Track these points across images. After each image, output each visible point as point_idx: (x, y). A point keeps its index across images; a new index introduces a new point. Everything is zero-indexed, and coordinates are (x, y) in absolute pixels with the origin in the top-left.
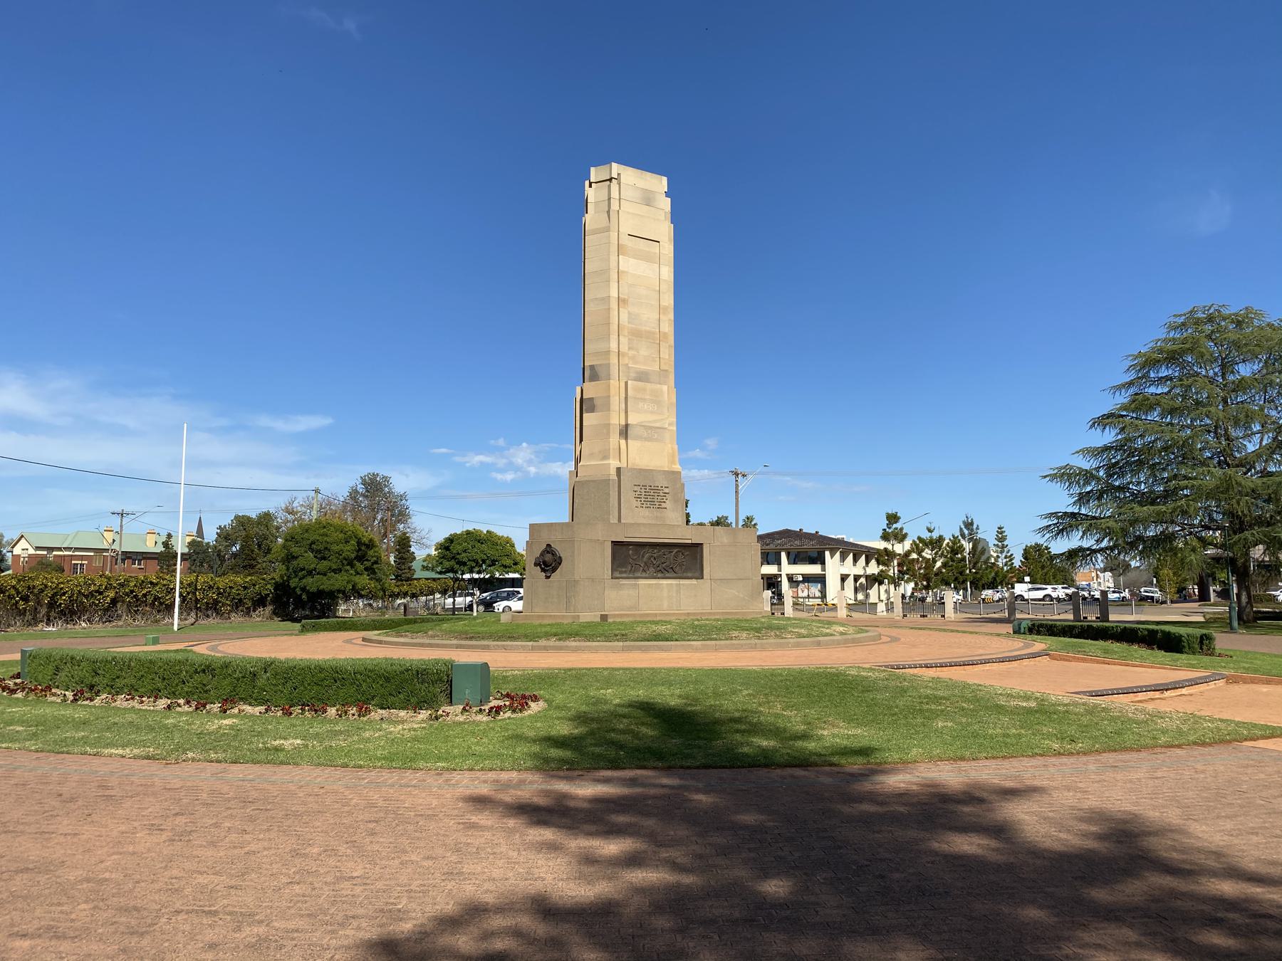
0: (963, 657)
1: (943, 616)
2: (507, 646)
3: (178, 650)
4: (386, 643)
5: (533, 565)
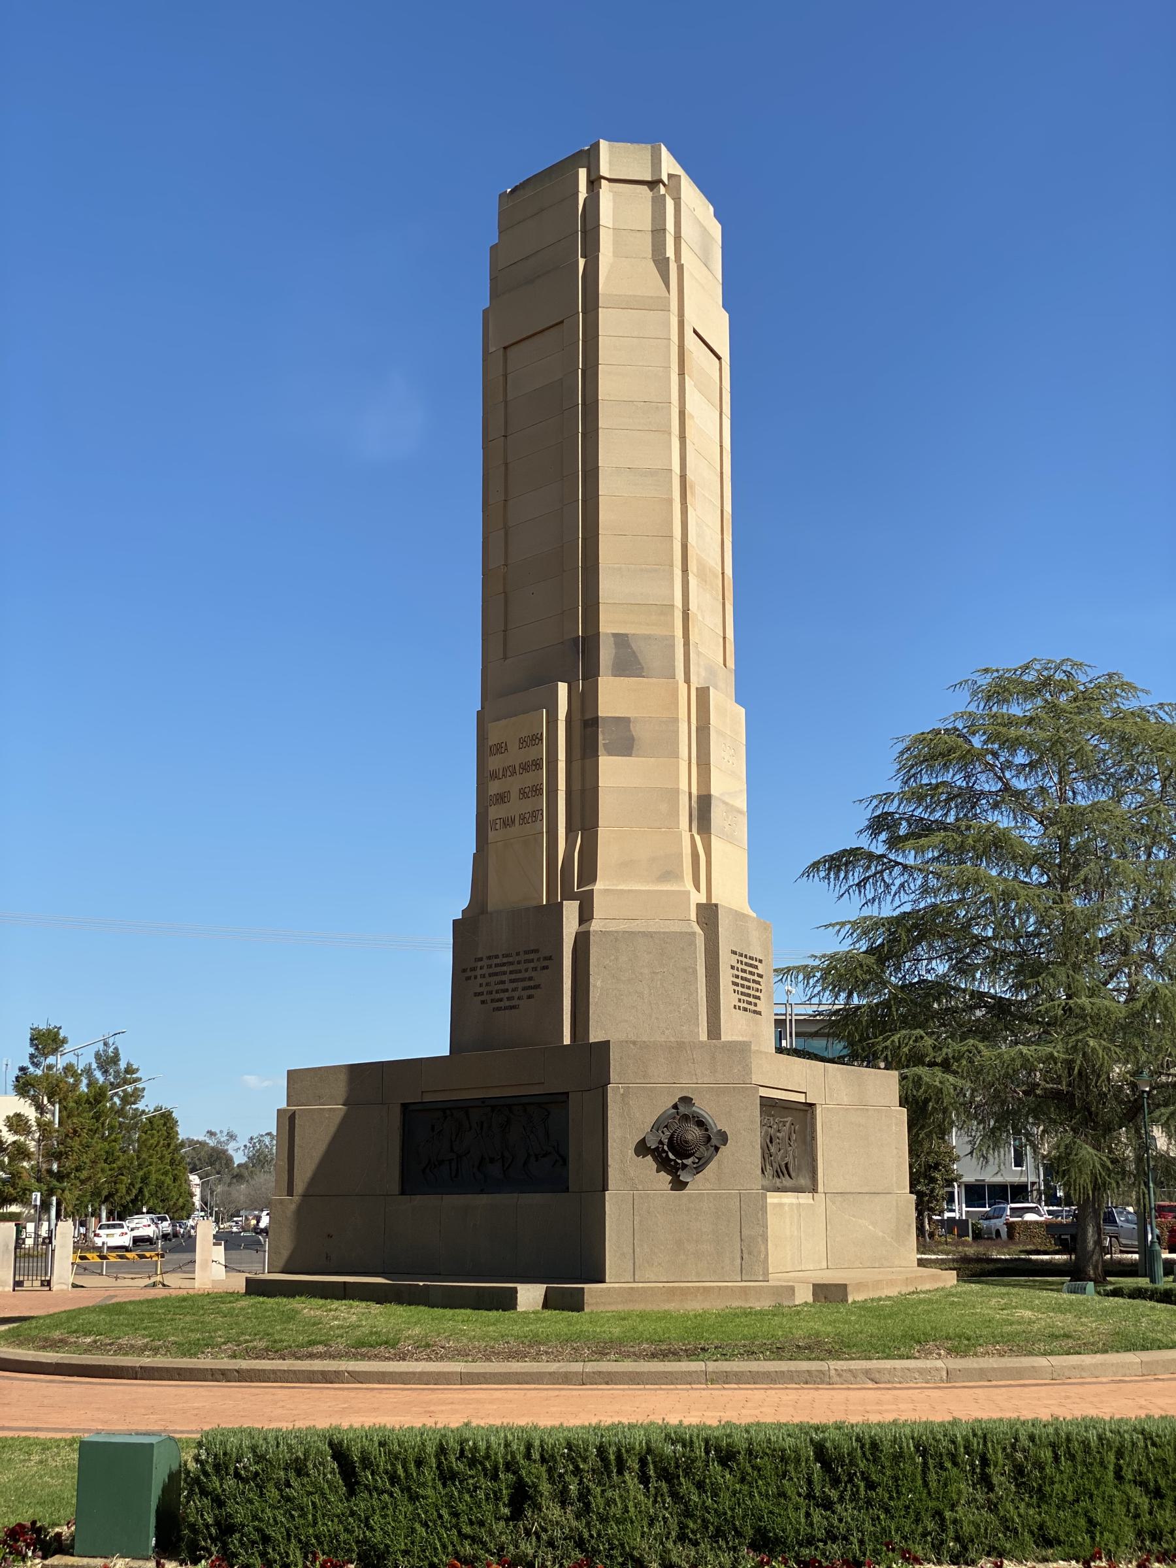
0: (478, 1389)
2: (879, 1371)
5: (631, 1152)
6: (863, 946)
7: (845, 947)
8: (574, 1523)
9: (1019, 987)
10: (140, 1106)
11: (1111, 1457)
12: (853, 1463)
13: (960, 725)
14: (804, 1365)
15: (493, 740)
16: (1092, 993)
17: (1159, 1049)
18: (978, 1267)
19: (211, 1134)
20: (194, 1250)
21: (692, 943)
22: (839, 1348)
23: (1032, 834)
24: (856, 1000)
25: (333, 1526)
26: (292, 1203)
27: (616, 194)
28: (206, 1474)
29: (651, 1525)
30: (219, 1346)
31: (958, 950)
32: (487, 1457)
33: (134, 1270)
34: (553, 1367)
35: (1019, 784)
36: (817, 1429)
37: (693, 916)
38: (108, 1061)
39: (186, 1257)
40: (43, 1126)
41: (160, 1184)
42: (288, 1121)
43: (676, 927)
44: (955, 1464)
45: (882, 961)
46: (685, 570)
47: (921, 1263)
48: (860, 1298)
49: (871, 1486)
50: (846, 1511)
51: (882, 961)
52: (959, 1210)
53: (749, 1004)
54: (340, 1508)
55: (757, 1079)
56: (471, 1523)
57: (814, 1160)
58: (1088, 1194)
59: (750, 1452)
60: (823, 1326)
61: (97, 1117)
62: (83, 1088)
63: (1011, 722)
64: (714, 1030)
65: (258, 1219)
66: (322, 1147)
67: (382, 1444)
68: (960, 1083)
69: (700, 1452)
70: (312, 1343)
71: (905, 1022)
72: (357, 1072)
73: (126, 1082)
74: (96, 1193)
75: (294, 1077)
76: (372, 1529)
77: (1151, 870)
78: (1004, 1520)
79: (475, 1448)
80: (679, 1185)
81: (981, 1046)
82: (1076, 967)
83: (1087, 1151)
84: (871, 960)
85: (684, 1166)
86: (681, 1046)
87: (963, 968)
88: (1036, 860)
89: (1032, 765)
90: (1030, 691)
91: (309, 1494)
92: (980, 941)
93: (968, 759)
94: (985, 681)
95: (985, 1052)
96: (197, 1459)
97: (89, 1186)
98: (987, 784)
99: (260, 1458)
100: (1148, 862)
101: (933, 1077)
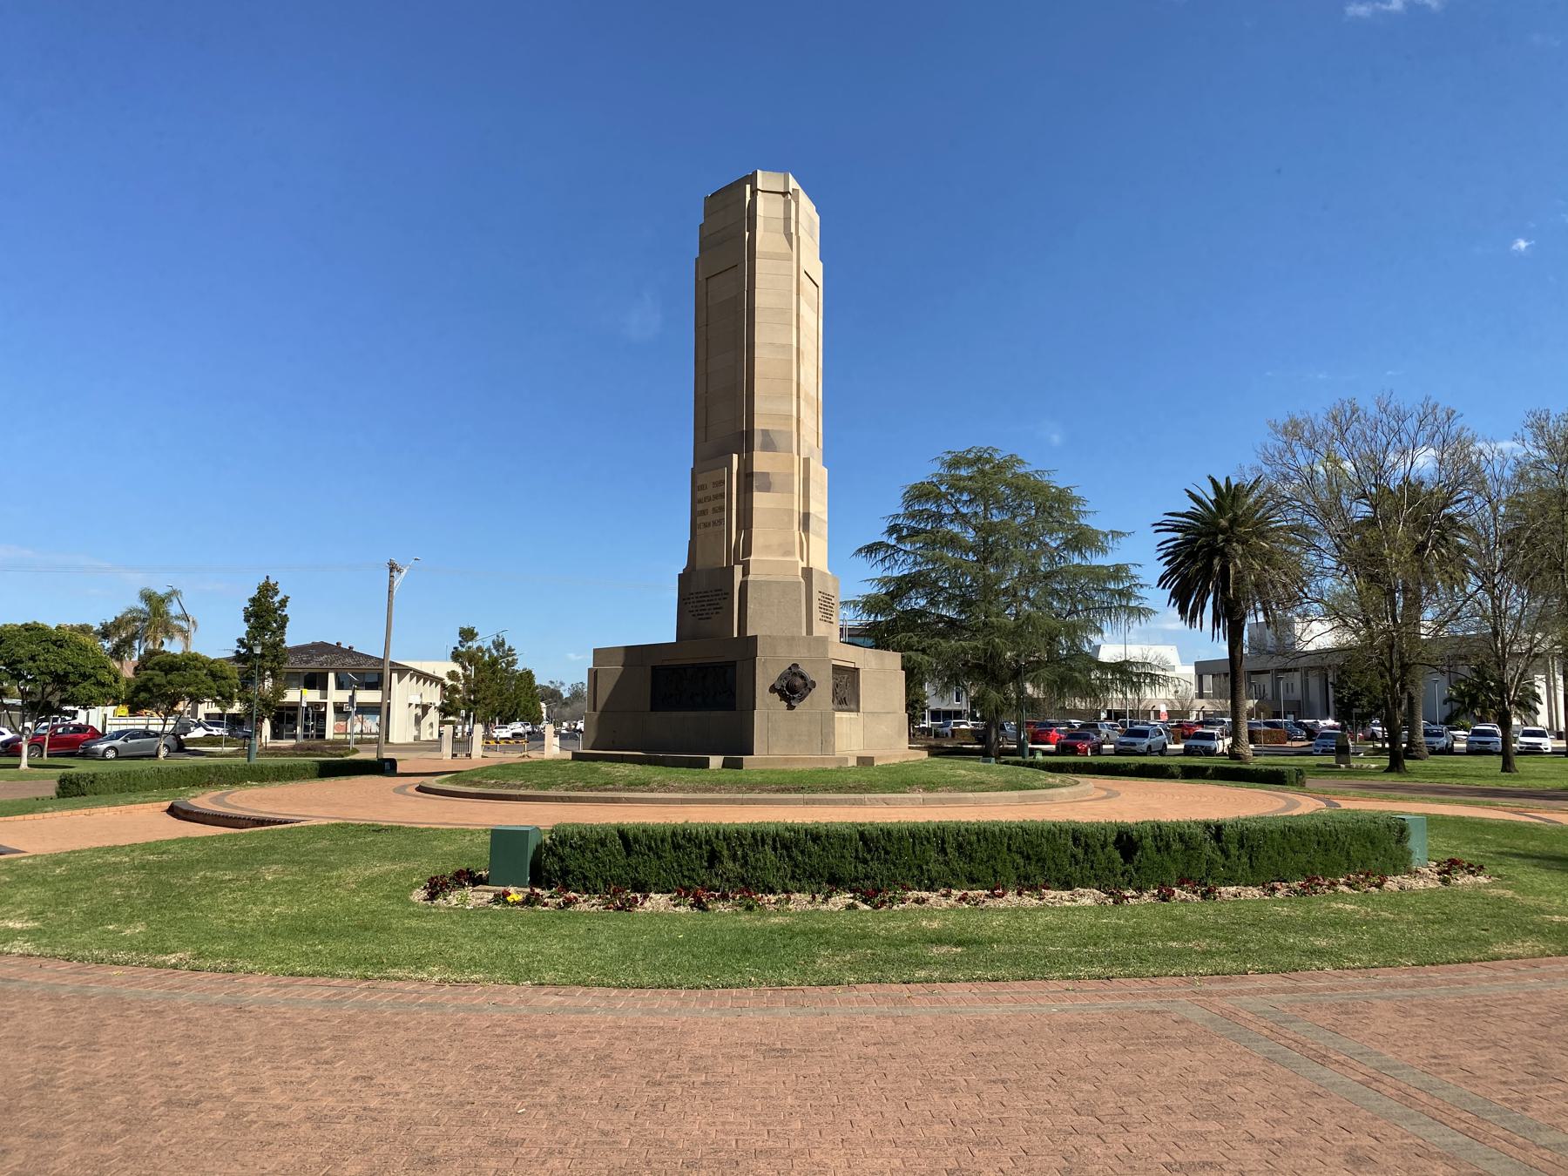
1: (469, 755)
2: (890, 799)
3: (115, 847)
4: (628, 800)
6: (884, 591)
7: (875, 591)
8: (740, 870)
9: (960, 613)
10: (516, 668)
11: (1006, 840)
12: (878, 842)
13: (935, 480)
14: (853, 796)
15: (699, 483)
16: (998, 615)
17: (1030, 644)
18: (936, 751)
19: (552, 682)
20: (544, 740)
21: (799, 587)
22: (870, 788)
23: (970, 536)
24: (879, 619)
25: (620, 871)
26: (596, 716)
27: (766, 199)
28: (555, 845)
29: (778, 871)
30: (559, 785)
31: (931, 593)
32: (697, 838)
33: (513, 749)
34: (728, 796)
35: (964, 510)
36: (860, 825)
37: (800, 574)
38: (499, 645)
39: (541, 743)
40: (466, 677)
41: (526, 708)
42: (594, 675)
43: (791, 579)
44: (929, 842)
45: (893, 599)
46: (798, 397)
47: (910, 748)
48: (880, 763)
49: (887, 853)
50: (875, 865)
51: (893, 599)
52: (928, 723)
53: (827, 617)
54: (623, 862)
55: (830, 656)
56: (688, 870)
57: (858, 696)
58: (1257, 511)
59: (827, 836)
61: (494, 673)
62: (486, 658)
63: (961, 478)
65: (576, 725)
66: (605, 700)
67: (644, 831)
68: (930, 660)
69: (802, 835)
70: (606, 784)
71: (904, 629)
72: (627, 648)
73: (508, 655)
74: (493, 711)
75: (596, 651)
76: (638, 873)
77: (1029, 554)
78: (952, 870)
79: (691, 833)
80: (791, 707)
81: (941, 641)
82: (990, 603)
83: (993, 694)
84: (888, 598)
85: (794, 698)
86: (793, 638)
87: (933, 603)
88: (972, 549)
89: (971, 501)
90: (970, 463)
91: (607, 855)
92: (943, 589)
93: (938, 497)
94: (948, 457)
95: (944, 645)
96: (551, 838)
97: (490, 707)
98: (947, 510)
99: (583, 838)
100: (1027, 551)
101: (918, 657)
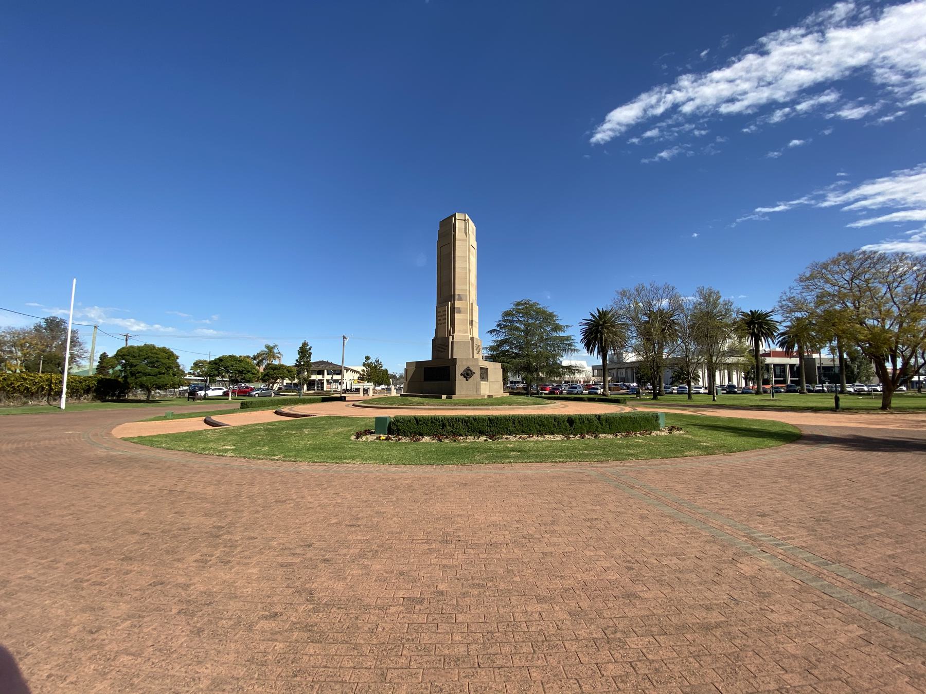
22: (492, 404)
23: (522, 327)
26: (407, 383)
33: (382, 393)
35: (521, 319)
38: (377, 361)
42: (406, 370)
50: (493, 428)
60: (489, 401)
63: (520, 309)
64: (473, 357)
80: (467, 380)
83: (530, 376)
86: (468, 359)
87: (511, 348)
90: (522, 305)
92: (514, 344)
94: (516, 303)
98: (515, 319)
99: (403, 420)
